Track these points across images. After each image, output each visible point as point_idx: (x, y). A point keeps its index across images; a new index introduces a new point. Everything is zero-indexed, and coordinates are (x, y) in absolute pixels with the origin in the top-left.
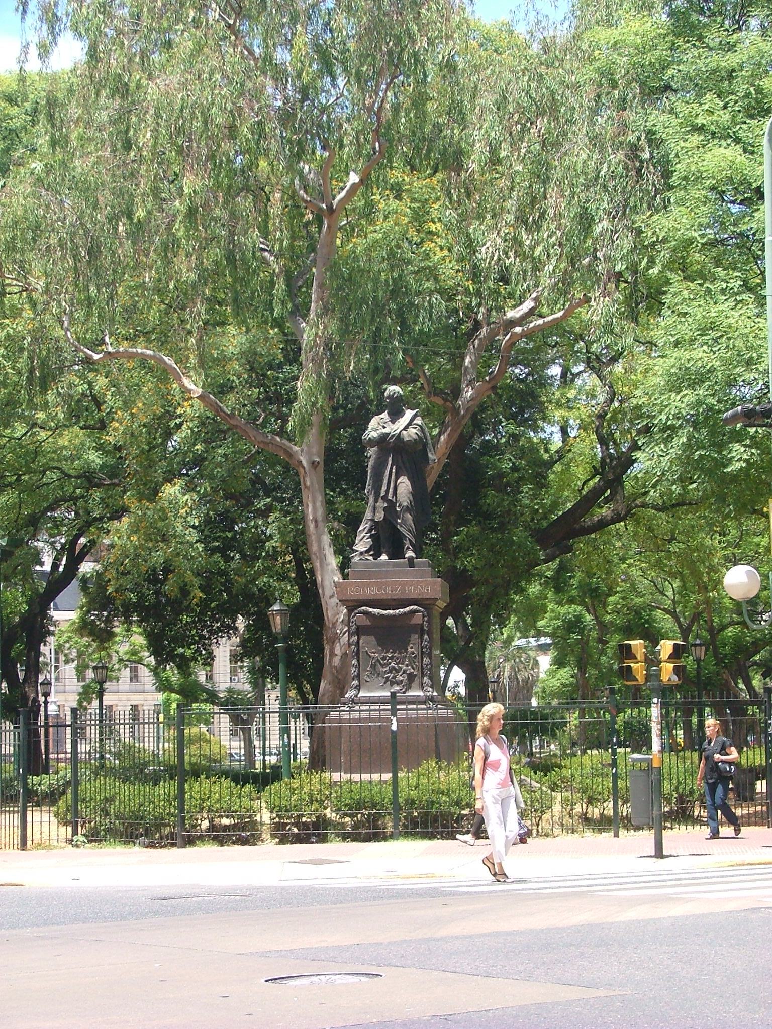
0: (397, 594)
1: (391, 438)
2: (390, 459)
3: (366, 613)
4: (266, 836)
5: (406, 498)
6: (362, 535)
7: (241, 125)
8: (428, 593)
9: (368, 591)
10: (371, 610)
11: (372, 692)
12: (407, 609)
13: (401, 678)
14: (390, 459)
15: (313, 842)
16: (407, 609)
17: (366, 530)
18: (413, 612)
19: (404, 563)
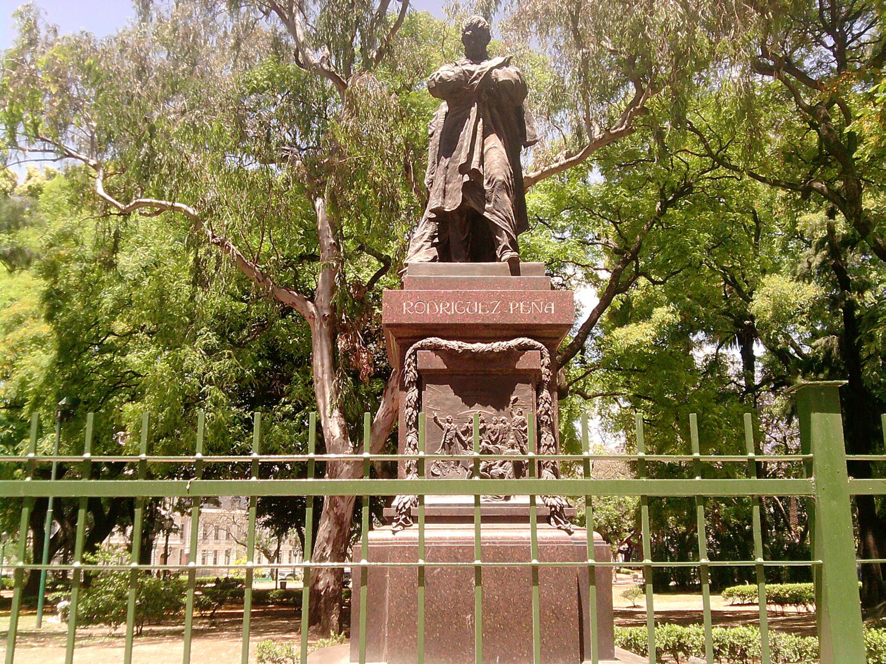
0: (494, 316)
1: (475, 78)
2: (474, 110)
3: (436, 349)
4: (189, 612)
5: (501, 170)
6: (418, 245)
7: (148, 394)
8: (550, 316)
9: (440, 309)
10: (444, 342)
11: (384, 599)
12: (513, 343)
13: (501, 470)
14: (474, 110)
15: (882, 428)
16: (513, 343)
17: (426, 237)
18: (524, 348)
19: (503, 268)
